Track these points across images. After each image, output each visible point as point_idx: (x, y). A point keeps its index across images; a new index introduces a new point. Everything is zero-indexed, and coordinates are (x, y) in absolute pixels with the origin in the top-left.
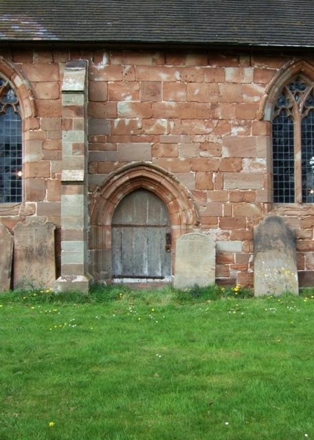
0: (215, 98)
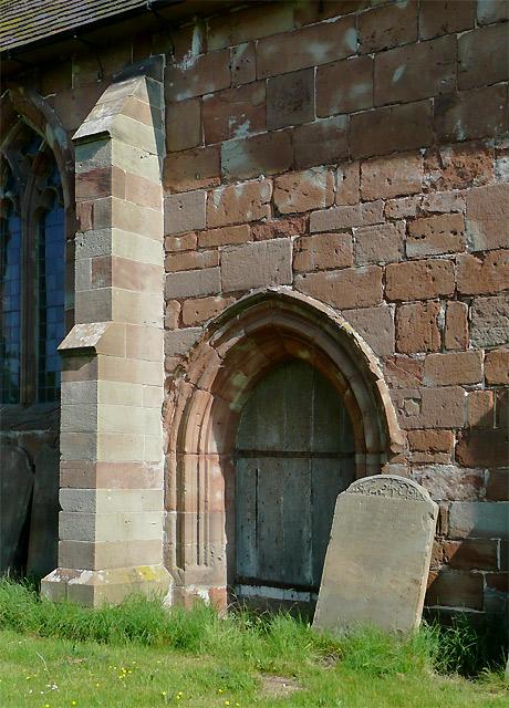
0: (447, 80)
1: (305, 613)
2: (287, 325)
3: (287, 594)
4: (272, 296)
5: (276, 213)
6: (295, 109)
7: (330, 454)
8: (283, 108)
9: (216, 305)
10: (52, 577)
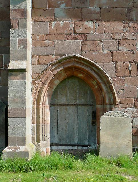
1: (96, 152)
2: (80, 66)
3: (69, 148)
4: (75, 57)
5: (75, 32)
6: (82, 3)
7: (84, 105)
8: (78, 2)
9: (53, 58)
10: (6, 150)
